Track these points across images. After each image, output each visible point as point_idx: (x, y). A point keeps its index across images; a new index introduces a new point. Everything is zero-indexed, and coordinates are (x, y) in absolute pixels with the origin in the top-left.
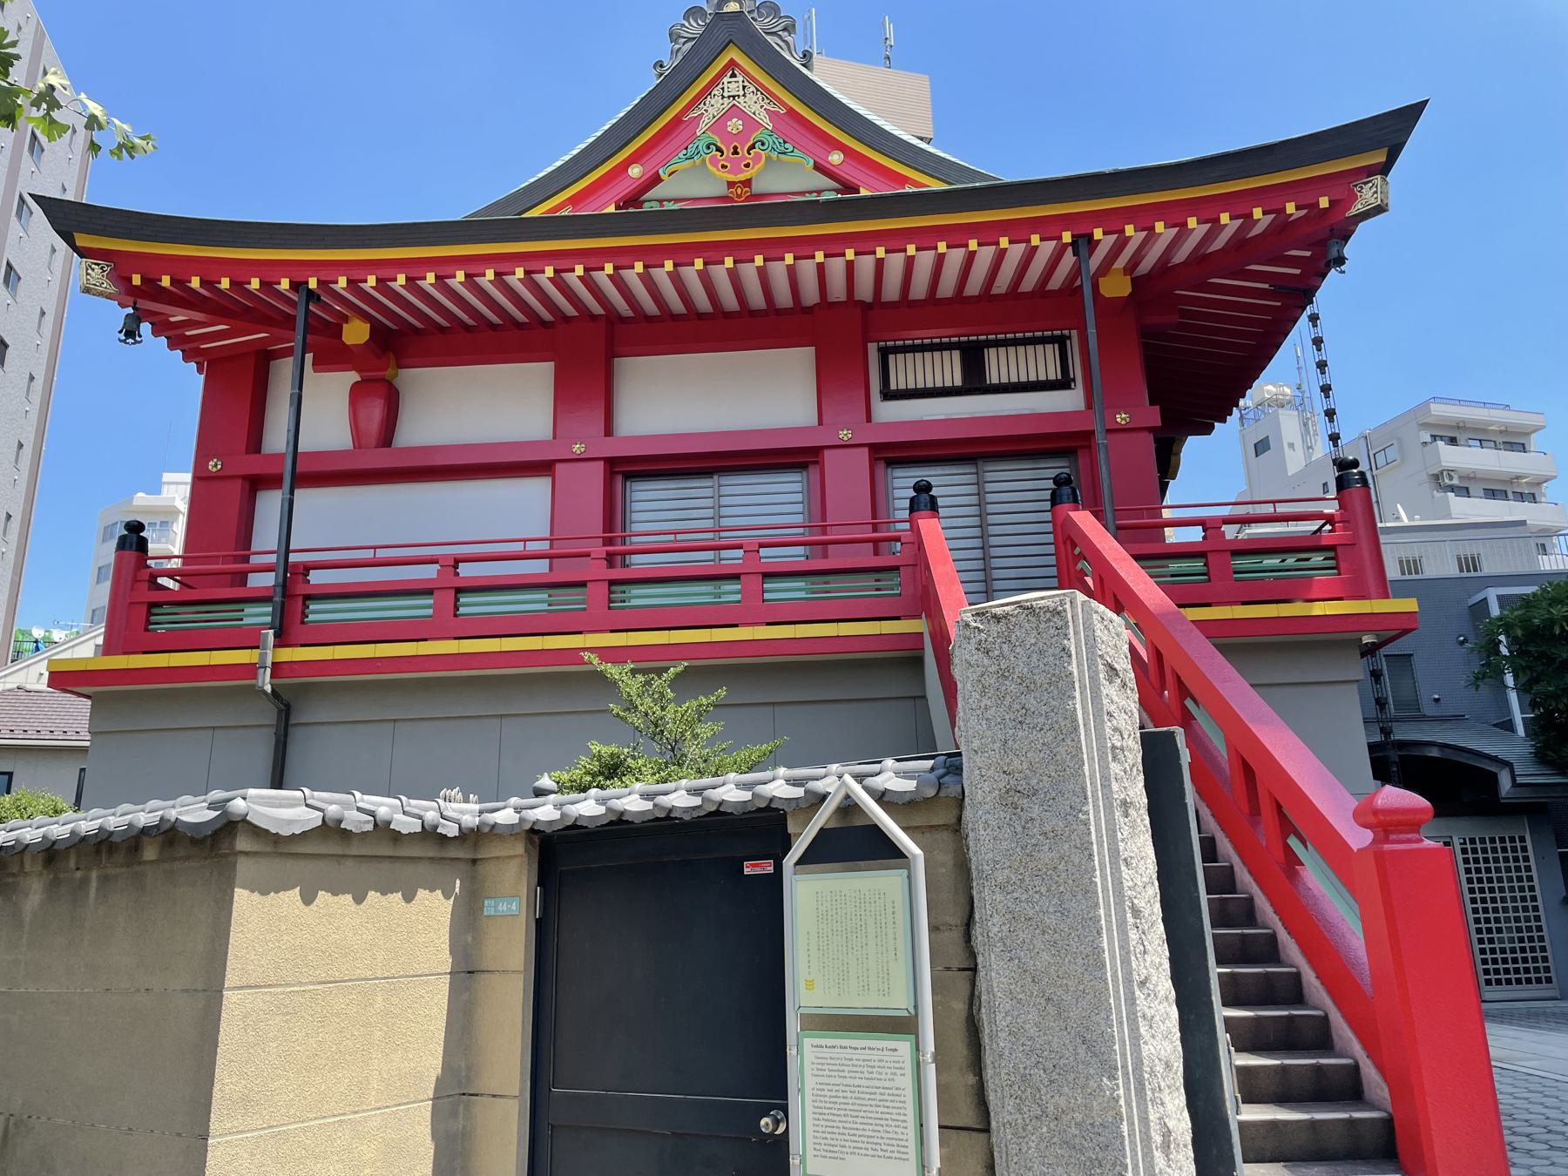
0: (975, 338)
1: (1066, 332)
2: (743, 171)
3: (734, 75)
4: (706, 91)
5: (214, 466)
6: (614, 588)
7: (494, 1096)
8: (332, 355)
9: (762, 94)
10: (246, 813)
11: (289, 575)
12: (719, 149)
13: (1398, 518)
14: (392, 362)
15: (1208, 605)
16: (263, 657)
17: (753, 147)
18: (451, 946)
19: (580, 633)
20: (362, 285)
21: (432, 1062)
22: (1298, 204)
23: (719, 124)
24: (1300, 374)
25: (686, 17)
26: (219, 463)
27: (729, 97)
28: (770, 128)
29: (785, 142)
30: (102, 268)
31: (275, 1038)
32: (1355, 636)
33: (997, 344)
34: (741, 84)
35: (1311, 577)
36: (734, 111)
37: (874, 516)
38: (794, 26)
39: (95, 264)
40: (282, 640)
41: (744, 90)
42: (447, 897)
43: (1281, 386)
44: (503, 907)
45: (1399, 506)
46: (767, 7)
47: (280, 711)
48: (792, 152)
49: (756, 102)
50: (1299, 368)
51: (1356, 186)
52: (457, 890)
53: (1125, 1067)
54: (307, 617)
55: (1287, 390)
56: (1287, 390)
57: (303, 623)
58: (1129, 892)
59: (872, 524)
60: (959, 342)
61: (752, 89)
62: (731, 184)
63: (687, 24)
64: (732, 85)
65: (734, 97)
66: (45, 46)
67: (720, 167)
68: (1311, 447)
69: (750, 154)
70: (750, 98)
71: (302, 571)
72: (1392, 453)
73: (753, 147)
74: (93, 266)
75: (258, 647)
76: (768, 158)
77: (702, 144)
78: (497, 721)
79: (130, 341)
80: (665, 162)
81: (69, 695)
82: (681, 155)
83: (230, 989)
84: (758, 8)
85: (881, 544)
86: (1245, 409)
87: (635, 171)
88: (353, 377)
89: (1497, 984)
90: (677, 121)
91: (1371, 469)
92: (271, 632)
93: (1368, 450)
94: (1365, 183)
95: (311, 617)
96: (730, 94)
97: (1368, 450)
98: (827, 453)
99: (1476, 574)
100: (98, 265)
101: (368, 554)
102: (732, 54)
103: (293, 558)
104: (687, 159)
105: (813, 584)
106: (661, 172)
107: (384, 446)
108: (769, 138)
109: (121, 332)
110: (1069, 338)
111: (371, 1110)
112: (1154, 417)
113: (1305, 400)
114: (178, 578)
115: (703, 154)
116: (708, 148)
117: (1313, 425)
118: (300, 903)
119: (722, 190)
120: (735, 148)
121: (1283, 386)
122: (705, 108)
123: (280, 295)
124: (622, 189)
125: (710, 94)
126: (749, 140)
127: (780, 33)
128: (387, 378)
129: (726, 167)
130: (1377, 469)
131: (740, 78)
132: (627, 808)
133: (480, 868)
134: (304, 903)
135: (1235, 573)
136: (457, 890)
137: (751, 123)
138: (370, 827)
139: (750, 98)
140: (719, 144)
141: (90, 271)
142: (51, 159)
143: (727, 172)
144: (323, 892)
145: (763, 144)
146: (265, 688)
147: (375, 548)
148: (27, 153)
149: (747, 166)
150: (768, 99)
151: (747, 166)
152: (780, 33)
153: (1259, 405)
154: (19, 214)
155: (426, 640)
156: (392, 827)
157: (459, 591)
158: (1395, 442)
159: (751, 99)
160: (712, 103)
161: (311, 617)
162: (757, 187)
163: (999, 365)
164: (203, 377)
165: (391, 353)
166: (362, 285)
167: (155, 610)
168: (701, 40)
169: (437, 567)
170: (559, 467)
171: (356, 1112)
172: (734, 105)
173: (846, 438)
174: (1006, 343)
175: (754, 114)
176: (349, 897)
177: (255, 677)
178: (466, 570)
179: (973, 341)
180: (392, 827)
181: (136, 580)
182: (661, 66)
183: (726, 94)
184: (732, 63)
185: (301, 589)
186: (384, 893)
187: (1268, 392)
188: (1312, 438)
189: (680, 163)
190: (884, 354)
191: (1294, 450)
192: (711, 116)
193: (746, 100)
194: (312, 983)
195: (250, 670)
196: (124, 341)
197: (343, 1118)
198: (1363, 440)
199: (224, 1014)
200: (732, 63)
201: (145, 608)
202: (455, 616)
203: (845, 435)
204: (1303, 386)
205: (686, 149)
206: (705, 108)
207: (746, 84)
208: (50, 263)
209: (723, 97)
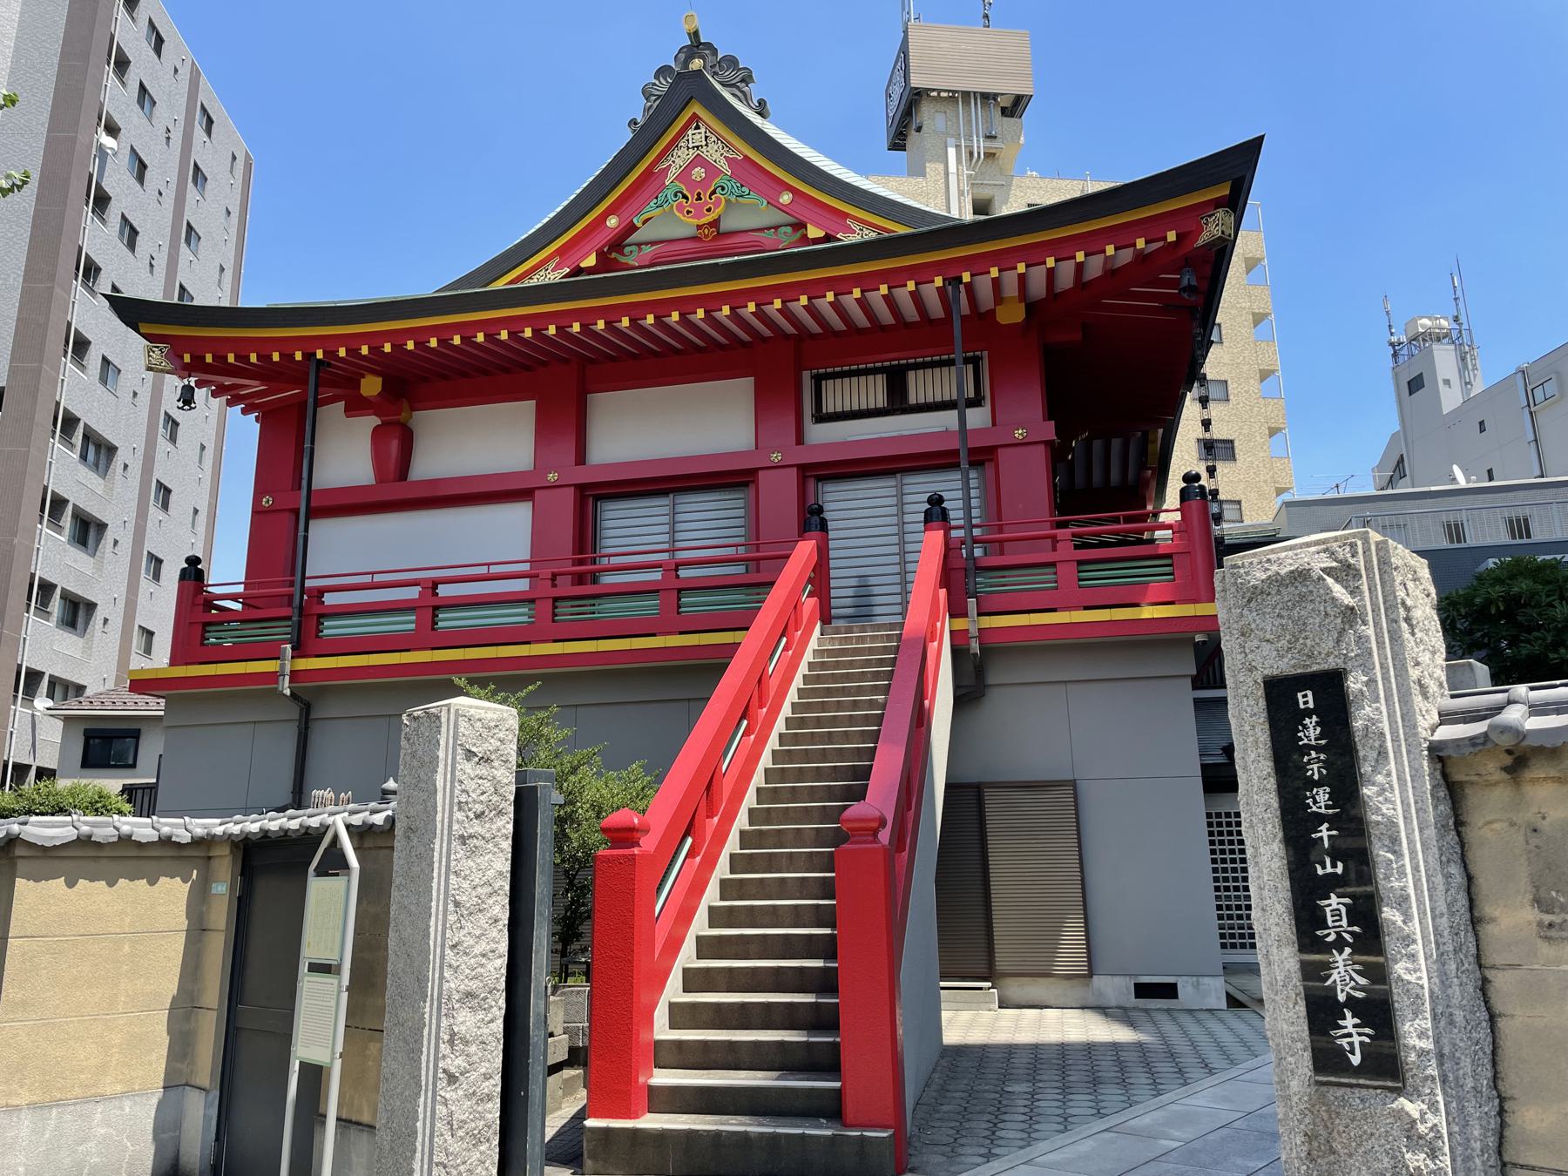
0: (929, 359)
1: (978, 353)
2: (705, 216)
3: (697, 127)
4: (673, 143)
5: (267, 501)
7: (208, 1009)
8: (357, 406)
9: (722, 142)
10: (19, 832)
11: (305, 597)
12: (685, 197)
13: (1454, 480)
14: (406, 405)
16: (282, 666)
17: (714, 192)
18: (187, 913)
19: (529, 643)
21: (170, 986)
22: (1179, 231)
23: (684, 176)
24: (1457, 305)
25: (657, 77)
26: (271, 499)
27: (693, 148)
28: (729, 174)
29: (742, 186)
30: (160, 350)
31: (45, 968)
32: (1191, 635)
33: (916, 367)
34: (703, 135)
35: (1147, 583)
36: (699, 161)
38: (751, 76)
39: (155, 347)
40: (300, 651)
41: (706, 140)
42: (185, 881)
43: (1437, 319)
44: (220, 888)
45: (1455, 468)
46: (727, 60)
47: (301, 709)
48: (749, 194)
49: (716, 151)
50: (1456, 299)
51: (1202, 218)
52: (194, 877)
53: (432, 995)
54: (322, 632)
55: (1444, 323)
56: (1444, 323)
57: (317, 637)
58: (453, 892)
59: (756, 544)
60: (883, 367)
61: (714, 138)
62: (699, 227)
63: (657, 83)
64: (695, 136)
65: (698, 147)
66: (201, 83)
67: (685, 212)
68: (1469, 383)
69: (711, 199)
70: (713, 147)
71: (316, 594)
72: (1551, 388)
73: (714, 192)
74: (154, 349)
75: (278, 658)
76: (728, 201)
77: (670, 193)
78: (1063, 687)
79: (186, 407)
80: (638, 212)
81: (146, 697)
82: (652, 204)
83: (12, 938)
84: (719, 62)
86: (1399, 345)
87: (612, 222)
88: (374, 421)
89: (1241, 948)
90: (648, 173)
91: (1529, 405)
92: (289, 646)
93: (1526, 385)
94: (1210, 216)
95: (326, 632)
96: (694, 145)
97: (1526, 385)
98: (760, 473)
99: (1529, 541)
100: (158, 347)
101: (367, 579)
102: (696, 108)
103: (308, 583)
104: (657, 207)
105: (747, 595)
106: (635, 221)
107: (400, 480)
108: (728, 183)
109: (179, 401)
110: (981, 358)
111: (119, 1014)
112: (1049, 431)
113: (1463, 332)
114: (241, 600)
115: (670, 201)
116: (676, 196)
117: (1472, 360)
118: (65, 887)
119: (691, 232)
120: (699, 194)
121: (1439, 318)
122: (673, 159)
124: (601, 239)
125: (677, 146)
126: (710, 187)
127: (739, 84)
128: (402, 421)
129: (691, 212)
130: (1535, 405)
131: (703, 130)
132: (291, 827)
133: (212, 861)
134: (67, 885)
135: (1080, 580)
136: (194, 877)
137: (712, 170)
138: (115, 839)
139: (713, 147)
140: (685, 192)
141: (151, 354)
142: (214, 186)
143: (691, 217)
144: (83, 880)
145: (723, 189)
146: (284, 692)
148: (192, 184)
149: (709, 210)
150: (727, 147)
151: (709, 210)
152: (739, 84)
153: (1413, 340)
154: (188, 241)
155: (408, 650)
156: (133, 838)
157: (436, 608)
158: (1553, 376)
159: (713, 148)
160: (679, 154)
161: (441, 624)
162: (726, 225)
163: (920, 387)
164: (259, 425)
165: (405, 400)
168: (665, 98)
169: (419, 588)
170: (537, 493)
171: (108, 1014)
172: (698, 154)
173: (776, 460)
174: (924, 366)
175: (715, 161)
176: (104, 883)
177: (277, 682)
178: (444, 591)
179: (896, 365)
180: (133, 838)
181: (194, 604)
182: (636, 124)
183: (690, 146)
184: (695, 117)
185: (317, 610)
186: (92, 880)
187: (1422, 326)
188: (1471, 373)
189: (651, 210)
190: (818, 380)
191: (1450, 387)
192: (678, 166)
193: (708, 149)
194: (74, 936)
195: (273, 677)
196: (182, 408)
197: (97, 1017)
198: (1520, 375)
199: (8, 952)
200: (695, 117)
201: (200, 628)
202: (433, 629)
203: (776, 457)
204: (1460, 317)
205: (657, 198)
206: (673, 159)
207: (708, 134)
208: (220, 281)
209: (688, 148)
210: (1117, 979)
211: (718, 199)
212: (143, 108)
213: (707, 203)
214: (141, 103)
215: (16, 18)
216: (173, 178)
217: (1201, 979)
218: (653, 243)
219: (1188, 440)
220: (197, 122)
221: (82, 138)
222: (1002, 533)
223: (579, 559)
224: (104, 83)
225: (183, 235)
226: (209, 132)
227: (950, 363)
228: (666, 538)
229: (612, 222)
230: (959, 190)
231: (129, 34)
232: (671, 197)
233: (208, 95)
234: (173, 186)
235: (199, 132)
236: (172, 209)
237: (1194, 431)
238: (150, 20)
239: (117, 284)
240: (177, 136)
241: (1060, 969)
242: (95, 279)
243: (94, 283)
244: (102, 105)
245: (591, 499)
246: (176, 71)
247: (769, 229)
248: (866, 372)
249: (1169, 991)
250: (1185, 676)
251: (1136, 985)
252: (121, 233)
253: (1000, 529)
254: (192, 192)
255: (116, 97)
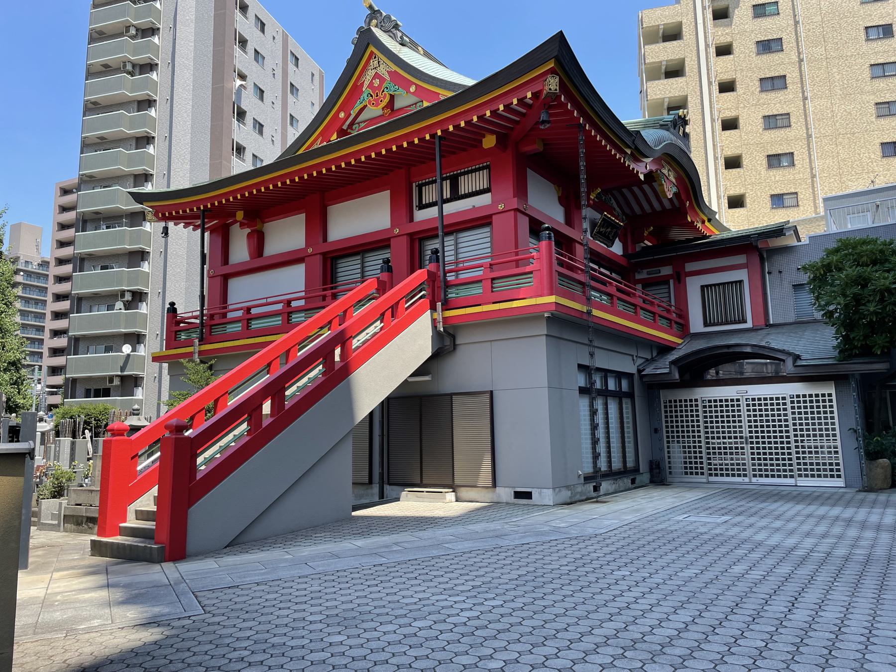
0: (448, 174)
6: (494, 282)
15: (480, 305)
16: (194, 349)
17: (383, 91)
20: (511, 106)
32: (542, 313)
36: (377, 76)
37: (516, 246)
40: (202, 341)
60: (446, 177)
73: (383, 91)
78: (489, 343)
82: (358, 102)
85: (520, 262)
95: (293, 320)
101: (264, 301)
109: (162, 234)
123: (474, 125)
147: (267, 298)
151: (381, 101)
154: (292, 124)
166: (511, 106)
167: (213, 328)
177: (193, 356)
178: (294, 304)
202: (288, 323)
210: (507, 489)
211: (385, 94)
212: (258, 62)
213: (380, 97)
214: (256, 60)
215: (193, 30)
216: (279, 93)
217: (542, 490)
218: (364, 122)
219: (874, 145)
220: (289, 62)
221: (227, 85)
222: (518, 255)
223: (223, 307)
224: (235, 55)
225: (289, 122)
226: (297, 65)
227: (435, 182)
228: (359, 275)
229: (342, 115)
230: (702, 7)
231: (244, 25)
232: (366, 96)
233: (294, 46)
234: (280, 98)
235: (291, 66)
236: (280, 109)
237: (878, 138)
238: (256, 15)
239: (255, 154)
240: (279, 72)
241: (480, 484)
242: (244, 153)
243: (243, 155)
244: (235, 66)
245: (329, 259)
246: (274, 38)
247: (412, 105)
248: (479, 169)
249: (528, 495)
250: (544, 335)
251: (515, 492)
252: (254, 127)
253: (517, 254)
254: (291, 99)
255: (242, 60)
